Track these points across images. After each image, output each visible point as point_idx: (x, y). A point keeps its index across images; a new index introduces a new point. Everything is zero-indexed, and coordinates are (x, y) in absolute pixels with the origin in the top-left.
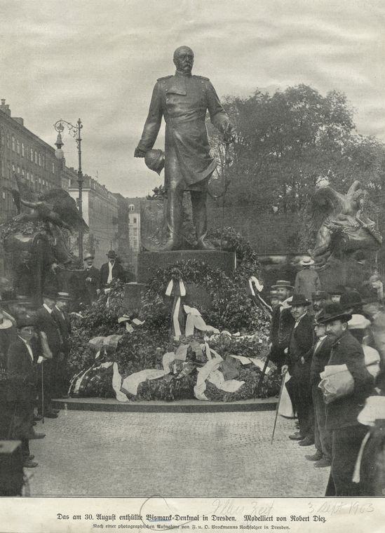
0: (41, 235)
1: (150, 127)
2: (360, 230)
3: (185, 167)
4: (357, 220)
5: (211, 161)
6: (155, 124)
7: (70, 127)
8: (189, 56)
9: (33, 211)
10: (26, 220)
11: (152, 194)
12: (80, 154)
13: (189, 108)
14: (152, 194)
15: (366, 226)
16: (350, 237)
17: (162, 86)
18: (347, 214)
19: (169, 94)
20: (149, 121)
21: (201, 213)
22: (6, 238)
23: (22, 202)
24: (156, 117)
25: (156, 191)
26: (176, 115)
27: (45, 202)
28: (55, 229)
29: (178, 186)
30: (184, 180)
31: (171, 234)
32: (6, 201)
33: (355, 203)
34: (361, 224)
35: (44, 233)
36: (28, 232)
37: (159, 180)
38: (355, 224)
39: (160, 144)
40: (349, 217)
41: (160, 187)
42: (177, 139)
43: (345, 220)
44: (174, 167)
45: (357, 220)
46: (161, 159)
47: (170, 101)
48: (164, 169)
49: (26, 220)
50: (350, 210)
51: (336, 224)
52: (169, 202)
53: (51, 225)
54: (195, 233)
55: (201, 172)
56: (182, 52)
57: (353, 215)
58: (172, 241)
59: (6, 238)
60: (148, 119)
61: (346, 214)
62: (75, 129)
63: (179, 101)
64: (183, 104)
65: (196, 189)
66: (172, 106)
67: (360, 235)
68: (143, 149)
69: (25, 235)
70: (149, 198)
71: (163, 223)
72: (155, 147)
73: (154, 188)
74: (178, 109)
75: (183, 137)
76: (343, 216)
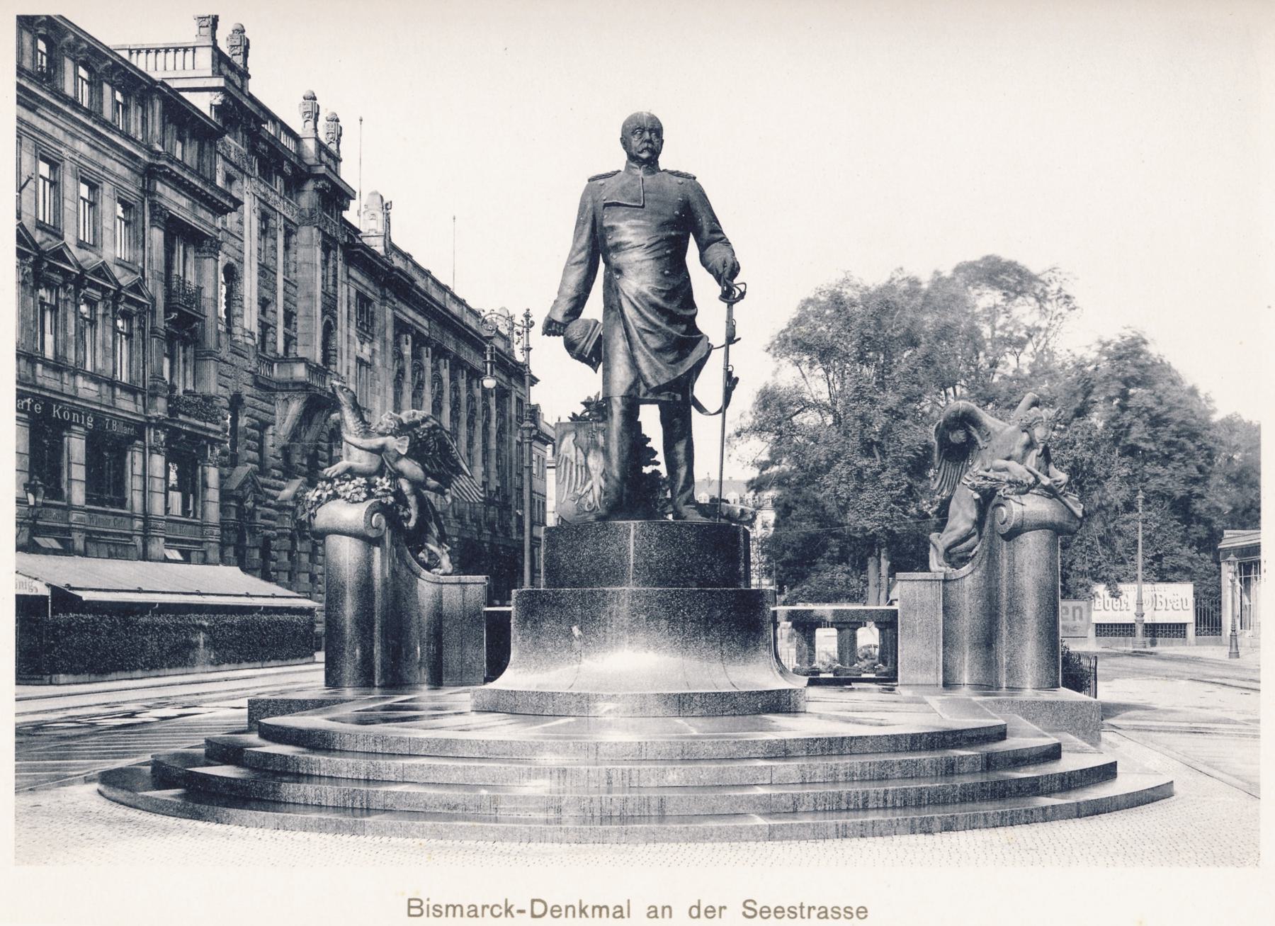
11: (580, 410)
14: (580, 410)
25: (587, 404)
39: (594, 309)
68: (559, 317)
70: (574, 418)
73: (584, 399)
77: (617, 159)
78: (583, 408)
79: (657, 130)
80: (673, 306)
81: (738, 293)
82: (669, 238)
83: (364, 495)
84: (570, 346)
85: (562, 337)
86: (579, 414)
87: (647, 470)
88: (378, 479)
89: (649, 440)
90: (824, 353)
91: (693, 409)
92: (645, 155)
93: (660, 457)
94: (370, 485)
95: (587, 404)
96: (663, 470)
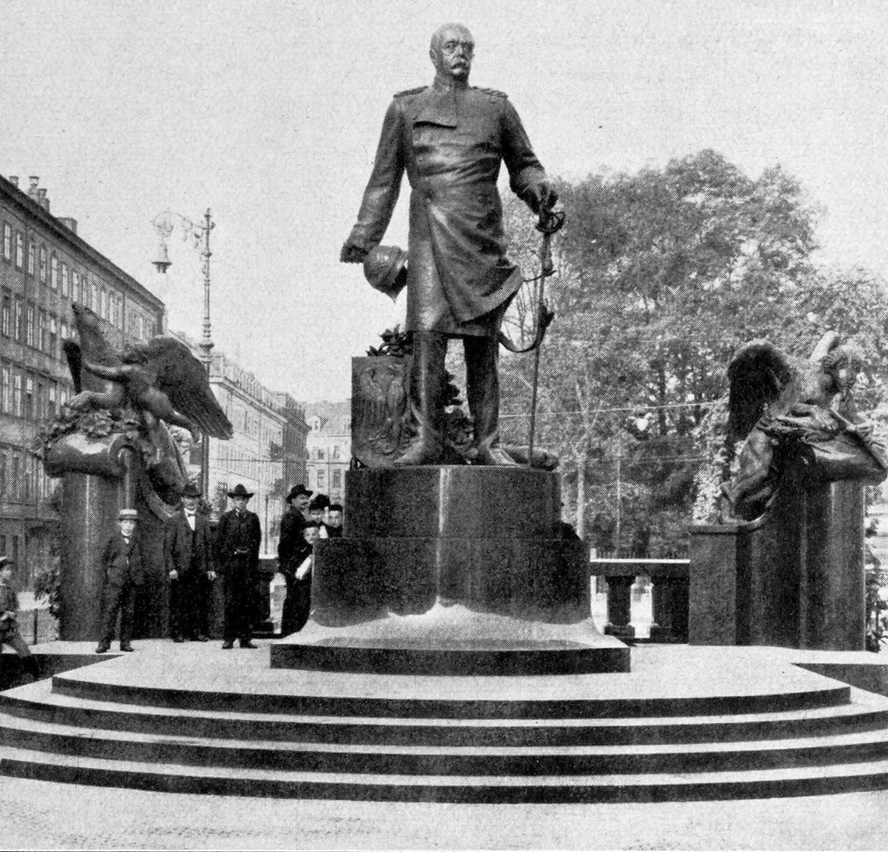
0: (128, 440)
1: (377, 195)
2: (840, 438)
3: (454, 282)
4: (833, 416)
5: (510, 271)
6: (385, 190)
7: (188, 225)
8: (464, 45)
9: (110, 386)
10: (94, 405)
11: (378, 343)
12: (207, 283)
13: (462, 155)
14: (378, 343)
15: (851, 427)
16: (816, 451)
17: (402, 107)
18: (810, 402)
19: (420, 125)
20: (373, 184)
21: (448, 81)
22: (49, 446)
23: (89, 370)
24: (389, 176)
25: (386, 337)
26: (433, 170)
27: (137, 368)
28: (157, 426)
29: (438, 324)
30: (452, 312)
31: (420, 430)
32: (35, 400)
33: (827, 378)
34: (842, 426)
35: (133, 434)
36: (100, 432)
37: (393, 312)
38: (829, 423)
39: (397, 233)
40: (813, 409)
41: (396, 329)
42: (436, 222)
43: (807, 414)
44: (428, 280)
45: (833, 416)
46: (399, 267)
47: (424, 138)
48: (405, 171)
49: (94, 405)
50: (818, 394)
51: (786, 423)
52: (417, 359)
53: (150, 419)
54: (472, 429)
55: (487, 294)
56: (450, 36)
57: (823, 404)
58: (421, 444)
59: (49, 446)
60: (374, 177)
61: (810, 402)
62: (199, 232)
63: (441, 141)
64: (457, 168)
65: (477, 332)
66: (424, 150)
67: (840, 450)
68: (360, 243)
69: (94, 437)
70: (373, 352)
71: (402, 406)
72: (387, 240)
73: (382, 332)
74: (438, 158)
75: (452, 220)
76: (803, 407)
77: (425, 75)
78: (381, 341)
79: (469, 47)
80: (486, 234)
81: (556, 221)
82: (482, 162)
83: (109, 429)
84: (370, 275)
85: (361, 265)
86: (377, 348)
87: (449, 409)
88: (123, 412)
89: (452, 377)
90: (224, 435)
91: (501, 345)
92: (456, 71)
93: (463, 395)
94: (116, 418)
95: (386, 337)
96: (465, 408)
